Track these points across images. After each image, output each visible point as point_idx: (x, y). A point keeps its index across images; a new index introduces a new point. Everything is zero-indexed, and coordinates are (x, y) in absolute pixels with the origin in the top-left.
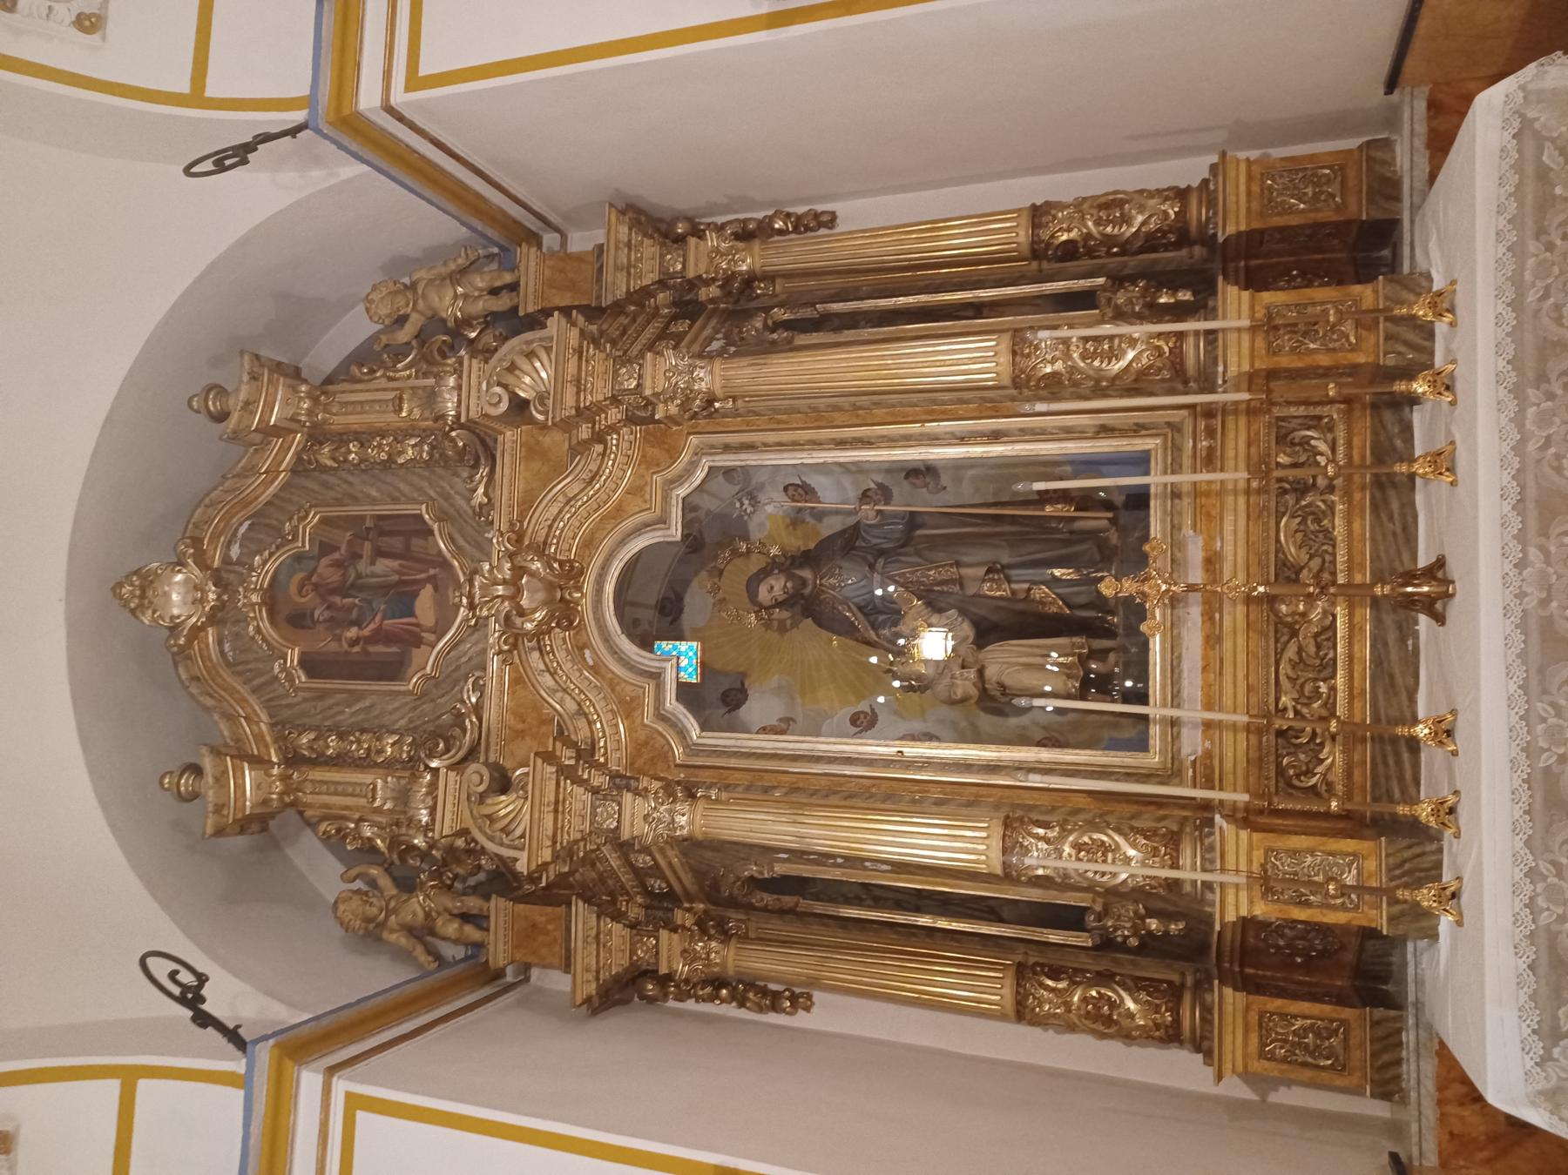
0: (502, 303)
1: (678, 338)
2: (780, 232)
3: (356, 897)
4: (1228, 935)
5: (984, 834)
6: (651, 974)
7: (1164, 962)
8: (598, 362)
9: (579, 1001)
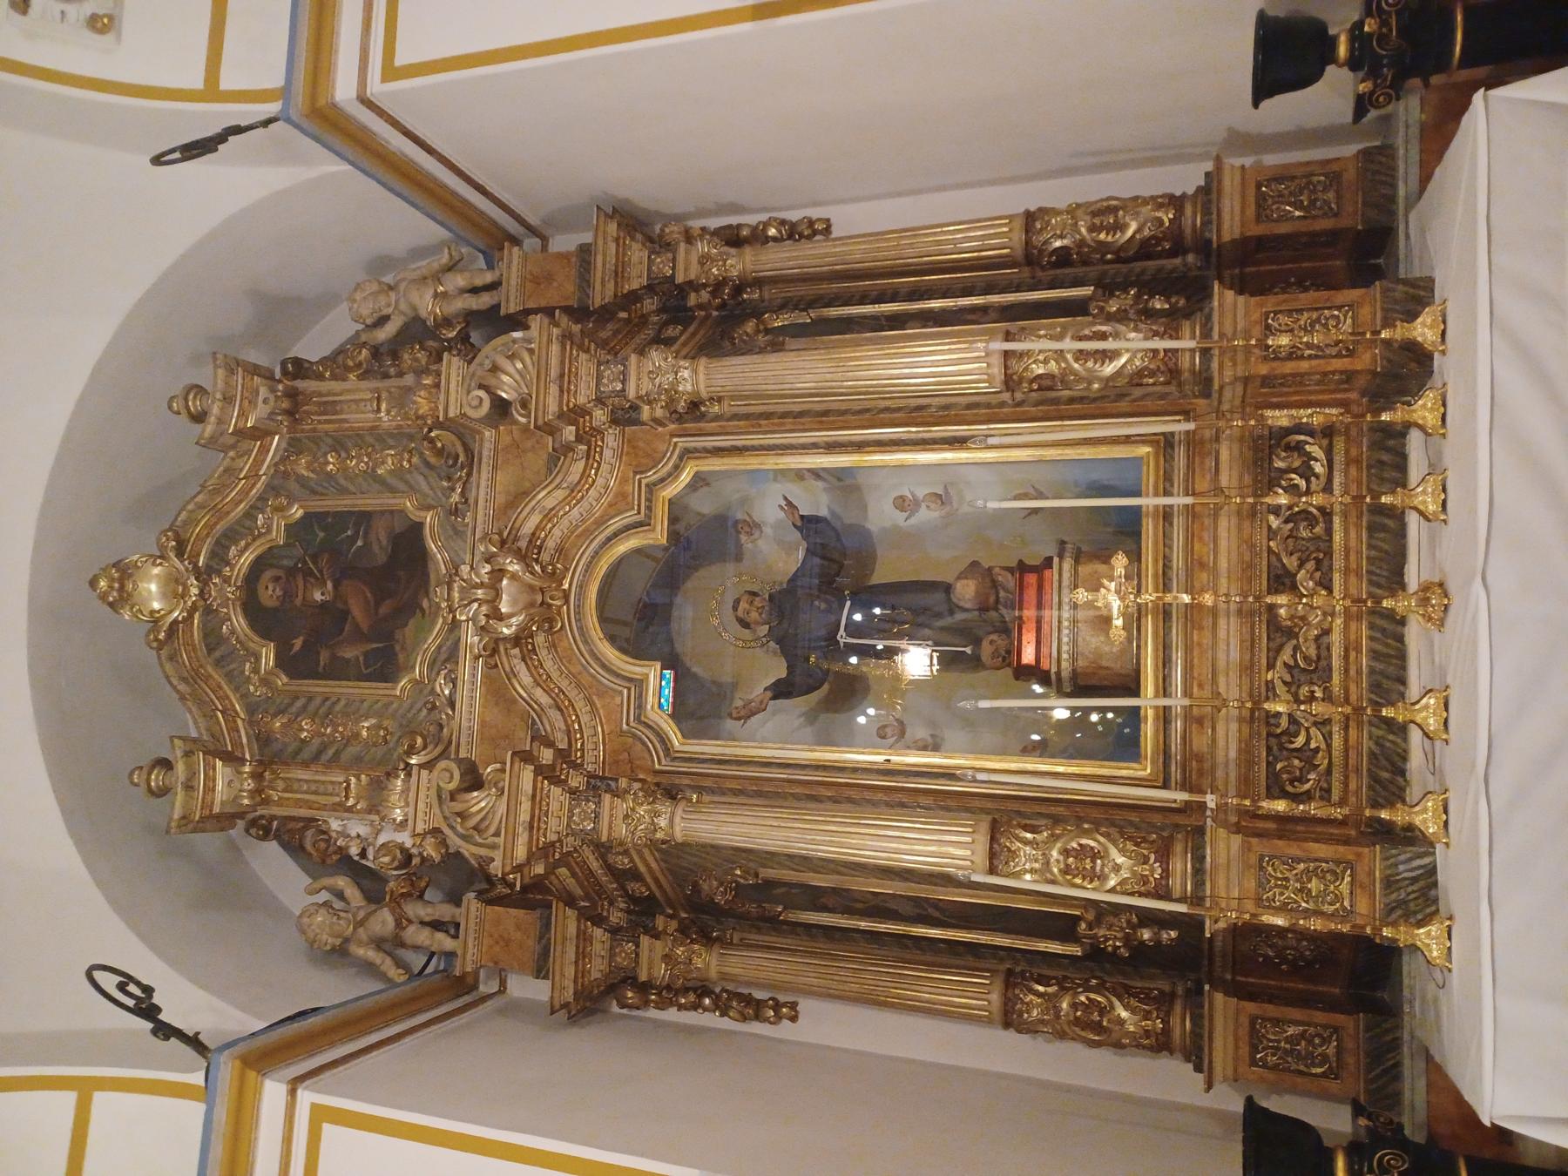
0: (484, 301)
1: (668, 342)
2: (775, 239)
3: (323, 911)
4: (1218, 944)
5: (969, 839)
6: (630, 980)
7: (1159, 972)
8: (585, 365)
9: (557, 1006)
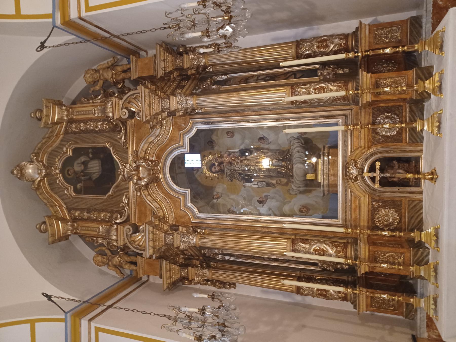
8: (156, 100)
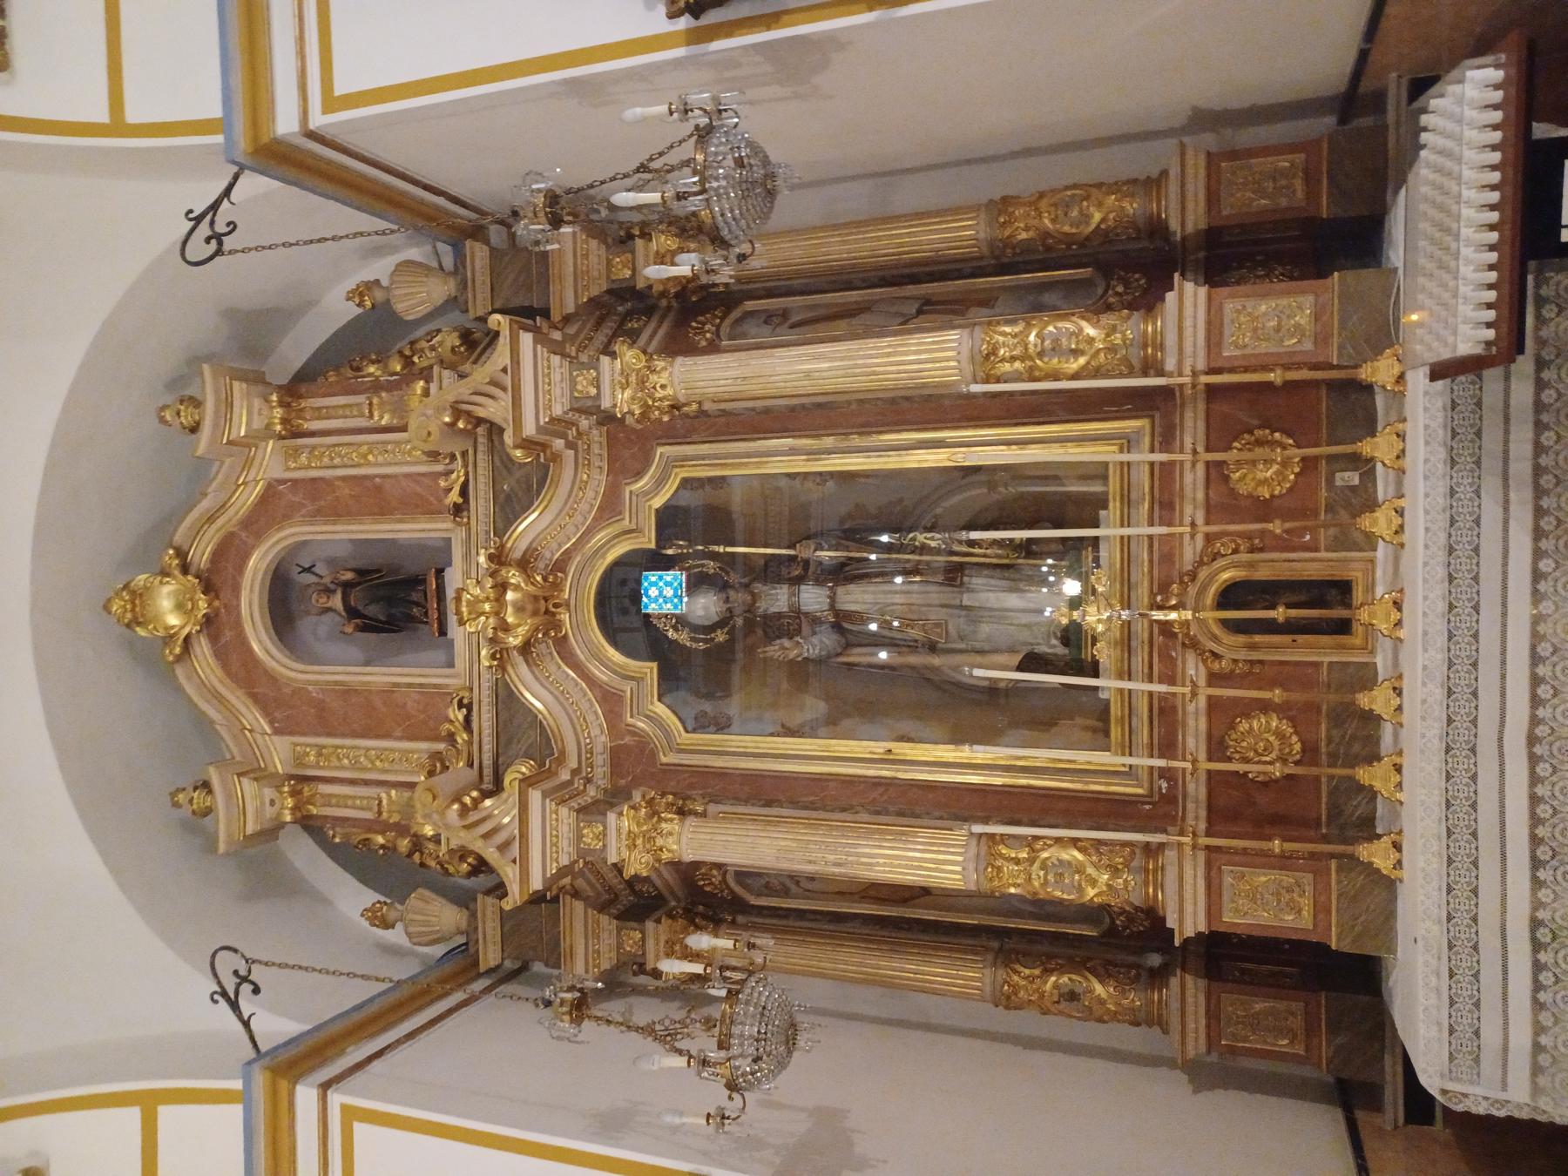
5: (960, 859)
